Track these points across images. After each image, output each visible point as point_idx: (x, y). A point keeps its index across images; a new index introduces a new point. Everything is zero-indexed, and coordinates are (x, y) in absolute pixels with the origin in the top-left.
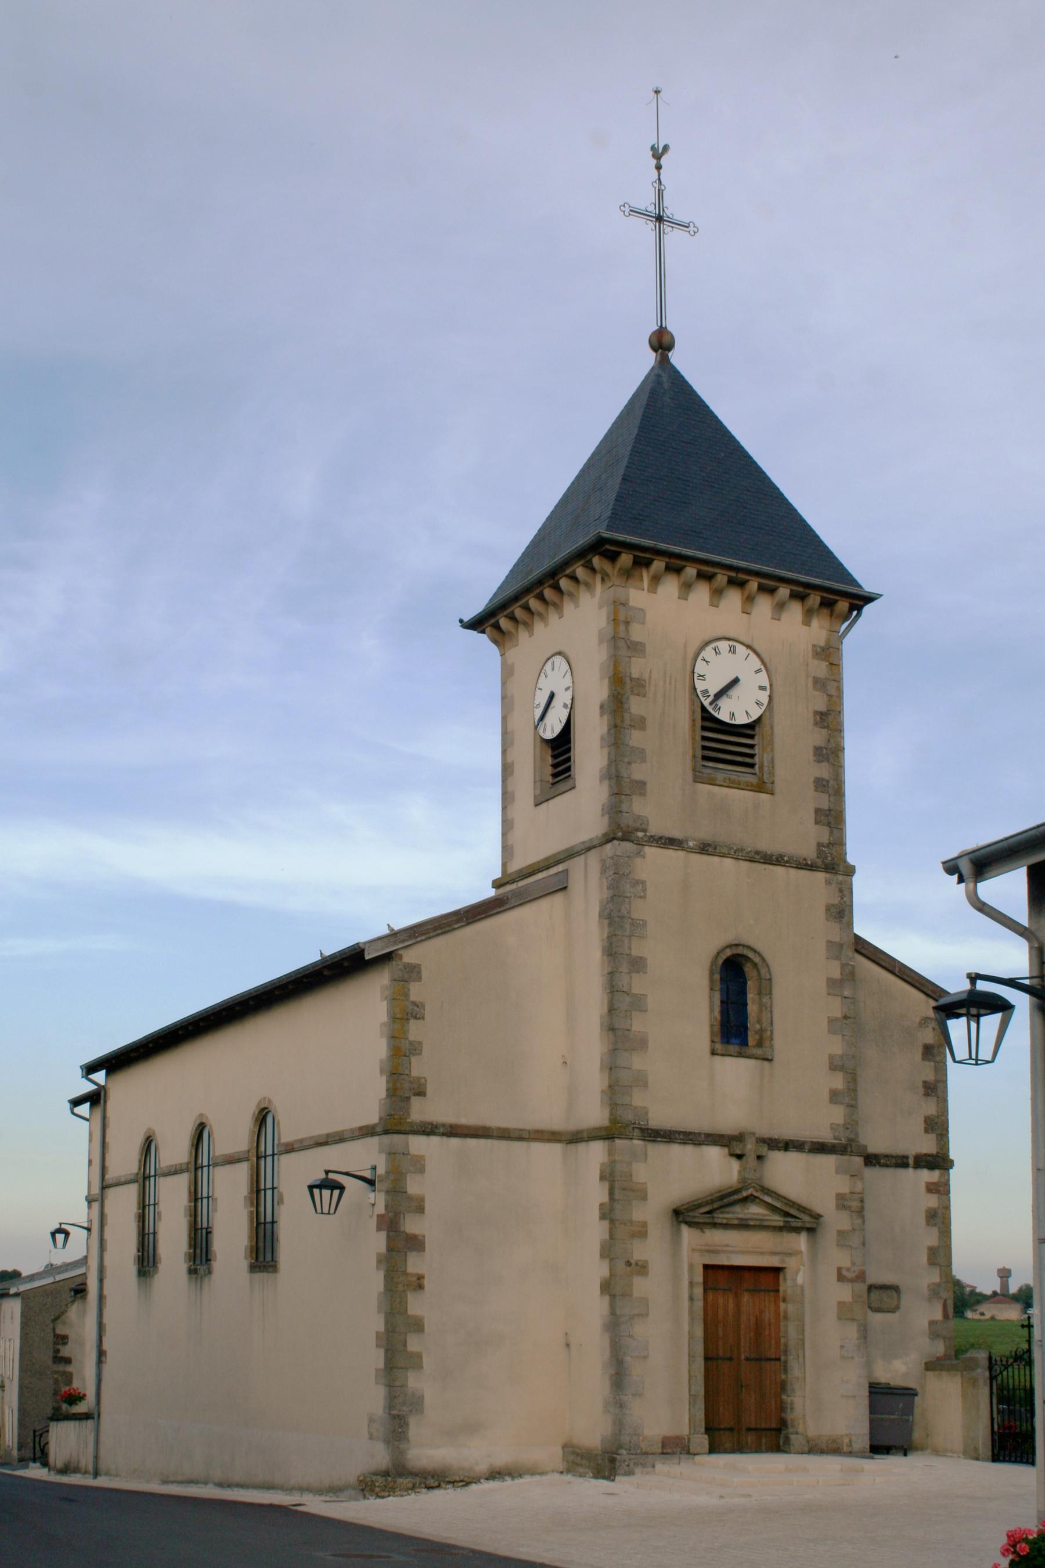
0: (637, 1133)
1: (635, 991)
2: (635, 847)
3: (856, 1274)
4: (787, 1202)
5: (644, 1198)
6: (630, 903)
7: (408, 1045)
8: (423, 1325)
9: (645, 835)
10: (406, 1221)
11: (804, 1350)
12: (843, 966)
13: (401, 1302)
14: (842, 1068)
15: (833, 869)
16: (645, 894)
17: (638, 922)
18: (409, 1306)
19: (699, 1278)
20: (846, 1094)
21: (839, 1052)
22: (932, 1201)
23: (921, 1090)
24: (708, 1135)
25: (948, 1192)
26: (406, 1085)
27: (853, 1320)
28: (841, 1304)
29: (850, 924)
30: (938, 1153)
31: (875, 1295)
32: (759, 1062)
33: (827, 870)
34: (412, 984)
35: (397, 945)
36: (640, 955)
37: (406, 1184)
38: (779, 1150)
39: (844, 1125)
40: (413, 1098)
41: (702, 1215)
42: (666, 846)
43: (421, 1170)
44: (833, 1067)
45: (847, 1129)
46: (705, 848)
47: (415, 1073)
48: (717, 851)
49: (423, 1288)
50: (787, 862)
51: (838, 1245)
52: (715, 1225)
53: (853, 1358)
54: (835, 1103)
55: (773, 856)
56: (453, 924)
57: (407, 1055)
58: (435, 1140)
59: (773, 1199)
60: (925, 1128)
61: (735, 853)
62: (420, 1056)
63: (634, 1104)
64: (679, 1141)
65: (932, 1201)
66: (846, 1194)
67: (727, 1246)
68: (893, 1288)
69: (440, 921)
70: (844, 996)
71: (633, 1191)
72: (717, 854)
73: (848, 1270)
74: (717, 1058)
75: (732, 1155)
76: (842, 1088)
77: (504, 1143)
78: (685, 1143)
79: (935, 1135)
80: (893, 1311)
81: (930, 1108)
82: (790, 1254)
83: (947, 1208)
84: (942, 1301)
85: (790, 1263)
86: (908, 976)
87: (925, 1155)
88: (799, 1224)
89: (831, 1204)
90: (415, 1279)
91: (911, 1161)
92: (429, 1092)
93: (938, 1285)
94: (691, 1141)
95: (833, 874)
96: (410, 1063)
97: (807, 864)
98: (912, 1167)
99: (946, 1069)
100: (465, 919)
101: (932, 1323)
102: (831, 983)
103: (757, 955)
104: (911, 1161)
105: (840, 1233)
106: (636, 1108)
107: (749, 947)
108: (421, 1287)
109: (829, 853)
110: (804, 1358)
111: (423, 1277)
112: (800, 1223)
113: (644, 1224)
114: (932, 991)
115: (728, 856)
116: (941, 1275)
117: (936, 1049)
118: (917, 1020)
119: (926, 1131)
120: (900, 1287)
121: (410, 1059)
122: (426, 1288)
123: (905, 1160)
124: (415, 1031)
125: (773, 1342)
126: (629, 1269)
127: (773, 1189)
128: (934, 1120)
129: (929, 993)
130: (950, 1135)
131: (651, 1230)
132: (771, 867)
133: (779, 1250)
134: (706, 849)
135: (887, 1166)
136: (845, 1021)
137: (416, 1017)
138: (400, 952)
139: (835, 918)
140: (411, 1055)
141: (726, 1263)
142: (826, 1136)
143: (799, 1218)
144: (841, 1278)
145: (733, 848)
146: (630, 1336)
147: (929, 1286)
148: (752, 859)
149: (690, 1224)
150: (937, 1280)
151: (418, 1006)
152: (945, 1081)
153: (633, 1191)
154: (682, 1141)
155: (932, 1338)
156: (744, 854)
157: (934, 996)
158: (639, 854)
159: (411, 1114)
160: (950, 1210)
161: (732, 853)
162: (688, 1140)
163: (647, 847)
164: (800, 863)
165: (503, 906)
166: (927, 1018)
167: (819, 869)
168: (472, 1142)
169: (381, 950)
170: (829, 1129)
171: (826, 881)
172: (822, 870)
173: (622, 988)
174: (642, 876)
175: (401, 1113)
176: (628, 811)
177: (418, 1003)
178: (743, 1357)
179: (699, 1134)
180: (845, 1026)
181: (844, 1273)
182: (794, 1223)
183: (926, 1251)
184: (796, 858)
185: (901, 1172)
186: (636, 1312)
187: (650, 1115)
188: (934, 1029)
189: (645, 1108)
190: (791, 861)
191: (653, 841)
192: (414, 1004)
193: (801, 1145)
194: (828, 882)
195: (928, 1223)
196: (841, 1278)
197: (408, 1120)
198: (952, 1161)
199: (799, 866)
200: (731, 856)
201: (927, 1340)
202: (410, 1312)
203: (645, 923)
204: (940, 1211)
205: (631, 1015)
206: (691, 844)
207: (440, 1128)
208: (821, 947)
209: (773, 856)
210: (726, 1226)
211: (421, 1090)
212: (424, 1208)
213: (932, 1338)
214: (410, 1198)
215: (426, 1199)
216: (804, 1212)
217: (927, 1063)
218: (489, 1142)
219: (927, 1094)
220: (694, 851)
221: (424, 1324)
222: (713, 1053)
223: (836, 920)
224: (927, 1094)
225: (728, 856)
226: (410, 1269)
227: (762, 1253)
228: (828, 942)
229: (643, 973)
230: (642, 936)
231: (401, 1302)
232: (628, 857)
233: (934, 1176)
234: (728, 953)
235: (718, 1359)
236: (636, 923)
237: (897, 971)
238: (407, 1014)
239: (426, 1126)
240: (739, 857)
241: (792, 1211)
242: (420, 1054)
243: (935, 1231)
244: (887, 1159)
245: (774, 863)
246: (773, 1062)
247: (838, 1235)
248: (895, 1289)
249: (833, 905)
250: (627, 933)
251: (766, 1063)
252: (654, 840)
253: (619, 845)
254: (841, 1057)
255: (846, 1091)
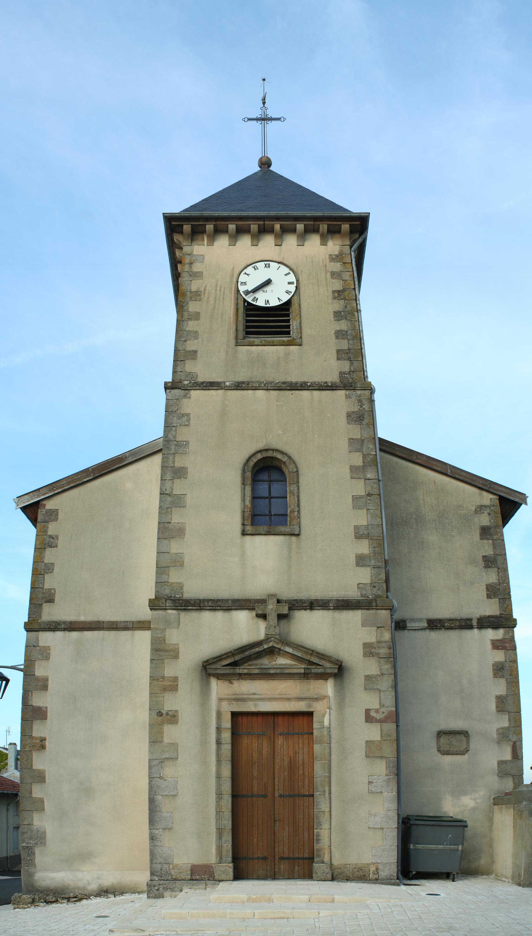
0: (169, 603)
1: (175, 492)
2: (183, 391)
3: (385, 714)
4: (305, 650)
5: (176, 656)
6: (176, 431)
7: (43, 567)
8: (45, 777)
9: (190, 382)
10: (34, 696)
11: (330, 787)
12: (364, 456)
13: (28, 759)
14: (367, 536)
15: (351, 386)
16: (189, 423)
17: (182, 443)
18: (34, 763)
19: (227, 724)
20: (372, 558)
21: (365, 523)
22: (500, 656)
23: (482, 563)
24: (235, 601)
25: (514, 648)
26: (40, 596)
27: (382, 757)
28: (368, 743)
29: (372, 424)
30: (501, 614)
31: (444, 740)
32: (287, 537)
33: (346, 388)
34: (50, 523)
35: (40, 497)
36: (182, 466)
37: (35, 669)
38: (306, 610)
39: (371, 584)
40: (44, 604)
41: (223, 667)
42: (207, 388)
43: (47, 658)
44: (359, 536)
45: (374, 587)
46: (239, 386)
47: (47, 586)
48: (250, 386)
49: (45, 748)
50: (310, 386)
51: (365, 689)
52: (241, 676)
53: (381, 792)
54: (362, 566)
55: (297, 383)
56: (83, 479)
57: (42, 574)
58: (59, 634)
59: (293, 650)
60: (487, 594)
61: (265, 385)
62: (52, 574)
63: (170, 581)
64: (208, 608)
65: (500, 656)
66: (373, 643)
67: (254, 694)
68: (462, 733)
69: (73, 478)
70: (367, 478)
71: (167, 651)
72: (249, 388)
73: (377, 711)
74: (248, 538)
75: (258, 616)
76: (368, 552)
77: (113, 633)
78: (215, 610)
79: (497, 600)
80: (462, 753)
81: (492, 577)
82: (317, 699)
83: (515, 661)
84: (512, 743)
85: (318, 707)
86: (460, 475)
87: (489, 616)
88: (320, 670)
89: (359, 651)
90: (38, 741)
91: (475, 623)
92: (57, 599)
93: (508, 729)
94: (220, 607)
95: (352, 391)
96: (44, 579)
97: (328, 386)
98: (477, 628)
99: (504, 545)
100: (92, 474)
101: (501, 763)
102: (354, 469)
103: (285, 456)
104: (475, 623)
105: (368, 678)
106: (172, 583)
107: (277, 450)
108: (43, 747)
109: (350, 378)
110: (330, 794)
111: (45, 740)
112: (321, 669)
113: (175, 679)
114: (482, 484)
115: (260, 388)
116: (510, 721)
117: (493, 529)
118: (473, 508)
119: (489, 597)
120: (470, 733)
121: (44, 577)
122: (47, 748)
123: (468, 622)
124: (49, 556)
125: (306, 780)
126: (160, 718)
127: (301, 644)
128: (496, 587)
129: (480, 486)
130: (513, 599)
131: (181, 684)
132: (297, 392)
133: (306, 695)
134: (240, 385)
135: (452, 628)
136: (369, 498)
137: (51, 546)
138: (44, 502)
139: (356, 421)
140: (45, 573)
141: (253, 709)
142: (353, 594)
143: (320, 665)
144: (369, 718)
145: (263, 382)
146: (161, 778)
147: (498, 730)
148: (280, 388)
149: (219, 677)
150: (506, 724)
151: (53, 538)
152: (504, 555)
153: (167, 651)
154: (211, 608)
155: (501, 776)
156: (272, 386)
157: (485, 488)
158: (185, 396)
159: (42, 616)
160: (517, 663)
161: (262, 385)
162: (217, 607)
163: (192, 391)
164: (321, 386)
165: (122, 462)
166: (482, 506)
167: (339, 388)
168: (88, 634)
169: (27, 502)
170: (356, 588)
171: (346, 396)
172: (341, 388)
173: (165, 491)
174: (188, 411)
175: (35, 616)
176: (182, 370)
177: (53, 536)
178: (277, 795)
179: (227, 600)
180: (369, 502)
181: (373, 714)
182: (315, 670)
183: (494, 699)
184: (318, 382)
185: (467, 634)
186: (167, 755)
187: (185, 589)
188: (489, 514)
189: (180, 583)
190: (314, 385)
191: (196, 385)
192: (51, 537)
193: (325, 603)
194: (347, 397)
195: (495, 676)
196: (369, 718)
197: (40, 621)
198: (515, 620)
199: (321, 388)
200: (261, 388)
201: (496, 778)
202: (34, 767)
203: (187, 442)
204: (507, 664)
205: (171, 511)
206: (228, 384)
207: (62, 625)
208: (344, 444)
209: (297, 383)
210: (251, 676)
211: (51, 598)
212: (47, 686)
213: (501, 776)
214: (38, 679)
215: (49, 680)
216: (324, 659)
217: (485, 541)
218: (101, 633)
219: (487, 567)
220: (230, 388)
221: (45, 776)
222: (244, 533)
223: (356, 423)
224: (487, 567)
225: (260, 388)
226: (34, 734)
227: (289, 699)
228: (350, 439)
229: (184, 478)
230: (185, 452)
231: (28, 759)
232: (177, 399)
233: (500, 634)
234: (259, 456)
235: (253, 796)
236: (181, 444)
237: (449, 472)
238: (45, 545)
239: (51, 624)
240: (269, 388)
241: (314, 659)
242: (52, 572)
243: (503, 682)
244: (451, 622)
245: (299, 388)
246: (301, 537)
247: (365, 679)
248: (465, 734)
249: (353, 412)
250: (172, 452)
251: (294, 538)
252: (197, 385)
253: (170, 392)
254: (367, 527)
255: (372, 554)
